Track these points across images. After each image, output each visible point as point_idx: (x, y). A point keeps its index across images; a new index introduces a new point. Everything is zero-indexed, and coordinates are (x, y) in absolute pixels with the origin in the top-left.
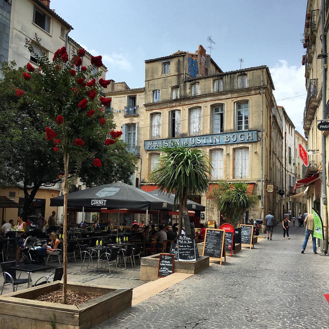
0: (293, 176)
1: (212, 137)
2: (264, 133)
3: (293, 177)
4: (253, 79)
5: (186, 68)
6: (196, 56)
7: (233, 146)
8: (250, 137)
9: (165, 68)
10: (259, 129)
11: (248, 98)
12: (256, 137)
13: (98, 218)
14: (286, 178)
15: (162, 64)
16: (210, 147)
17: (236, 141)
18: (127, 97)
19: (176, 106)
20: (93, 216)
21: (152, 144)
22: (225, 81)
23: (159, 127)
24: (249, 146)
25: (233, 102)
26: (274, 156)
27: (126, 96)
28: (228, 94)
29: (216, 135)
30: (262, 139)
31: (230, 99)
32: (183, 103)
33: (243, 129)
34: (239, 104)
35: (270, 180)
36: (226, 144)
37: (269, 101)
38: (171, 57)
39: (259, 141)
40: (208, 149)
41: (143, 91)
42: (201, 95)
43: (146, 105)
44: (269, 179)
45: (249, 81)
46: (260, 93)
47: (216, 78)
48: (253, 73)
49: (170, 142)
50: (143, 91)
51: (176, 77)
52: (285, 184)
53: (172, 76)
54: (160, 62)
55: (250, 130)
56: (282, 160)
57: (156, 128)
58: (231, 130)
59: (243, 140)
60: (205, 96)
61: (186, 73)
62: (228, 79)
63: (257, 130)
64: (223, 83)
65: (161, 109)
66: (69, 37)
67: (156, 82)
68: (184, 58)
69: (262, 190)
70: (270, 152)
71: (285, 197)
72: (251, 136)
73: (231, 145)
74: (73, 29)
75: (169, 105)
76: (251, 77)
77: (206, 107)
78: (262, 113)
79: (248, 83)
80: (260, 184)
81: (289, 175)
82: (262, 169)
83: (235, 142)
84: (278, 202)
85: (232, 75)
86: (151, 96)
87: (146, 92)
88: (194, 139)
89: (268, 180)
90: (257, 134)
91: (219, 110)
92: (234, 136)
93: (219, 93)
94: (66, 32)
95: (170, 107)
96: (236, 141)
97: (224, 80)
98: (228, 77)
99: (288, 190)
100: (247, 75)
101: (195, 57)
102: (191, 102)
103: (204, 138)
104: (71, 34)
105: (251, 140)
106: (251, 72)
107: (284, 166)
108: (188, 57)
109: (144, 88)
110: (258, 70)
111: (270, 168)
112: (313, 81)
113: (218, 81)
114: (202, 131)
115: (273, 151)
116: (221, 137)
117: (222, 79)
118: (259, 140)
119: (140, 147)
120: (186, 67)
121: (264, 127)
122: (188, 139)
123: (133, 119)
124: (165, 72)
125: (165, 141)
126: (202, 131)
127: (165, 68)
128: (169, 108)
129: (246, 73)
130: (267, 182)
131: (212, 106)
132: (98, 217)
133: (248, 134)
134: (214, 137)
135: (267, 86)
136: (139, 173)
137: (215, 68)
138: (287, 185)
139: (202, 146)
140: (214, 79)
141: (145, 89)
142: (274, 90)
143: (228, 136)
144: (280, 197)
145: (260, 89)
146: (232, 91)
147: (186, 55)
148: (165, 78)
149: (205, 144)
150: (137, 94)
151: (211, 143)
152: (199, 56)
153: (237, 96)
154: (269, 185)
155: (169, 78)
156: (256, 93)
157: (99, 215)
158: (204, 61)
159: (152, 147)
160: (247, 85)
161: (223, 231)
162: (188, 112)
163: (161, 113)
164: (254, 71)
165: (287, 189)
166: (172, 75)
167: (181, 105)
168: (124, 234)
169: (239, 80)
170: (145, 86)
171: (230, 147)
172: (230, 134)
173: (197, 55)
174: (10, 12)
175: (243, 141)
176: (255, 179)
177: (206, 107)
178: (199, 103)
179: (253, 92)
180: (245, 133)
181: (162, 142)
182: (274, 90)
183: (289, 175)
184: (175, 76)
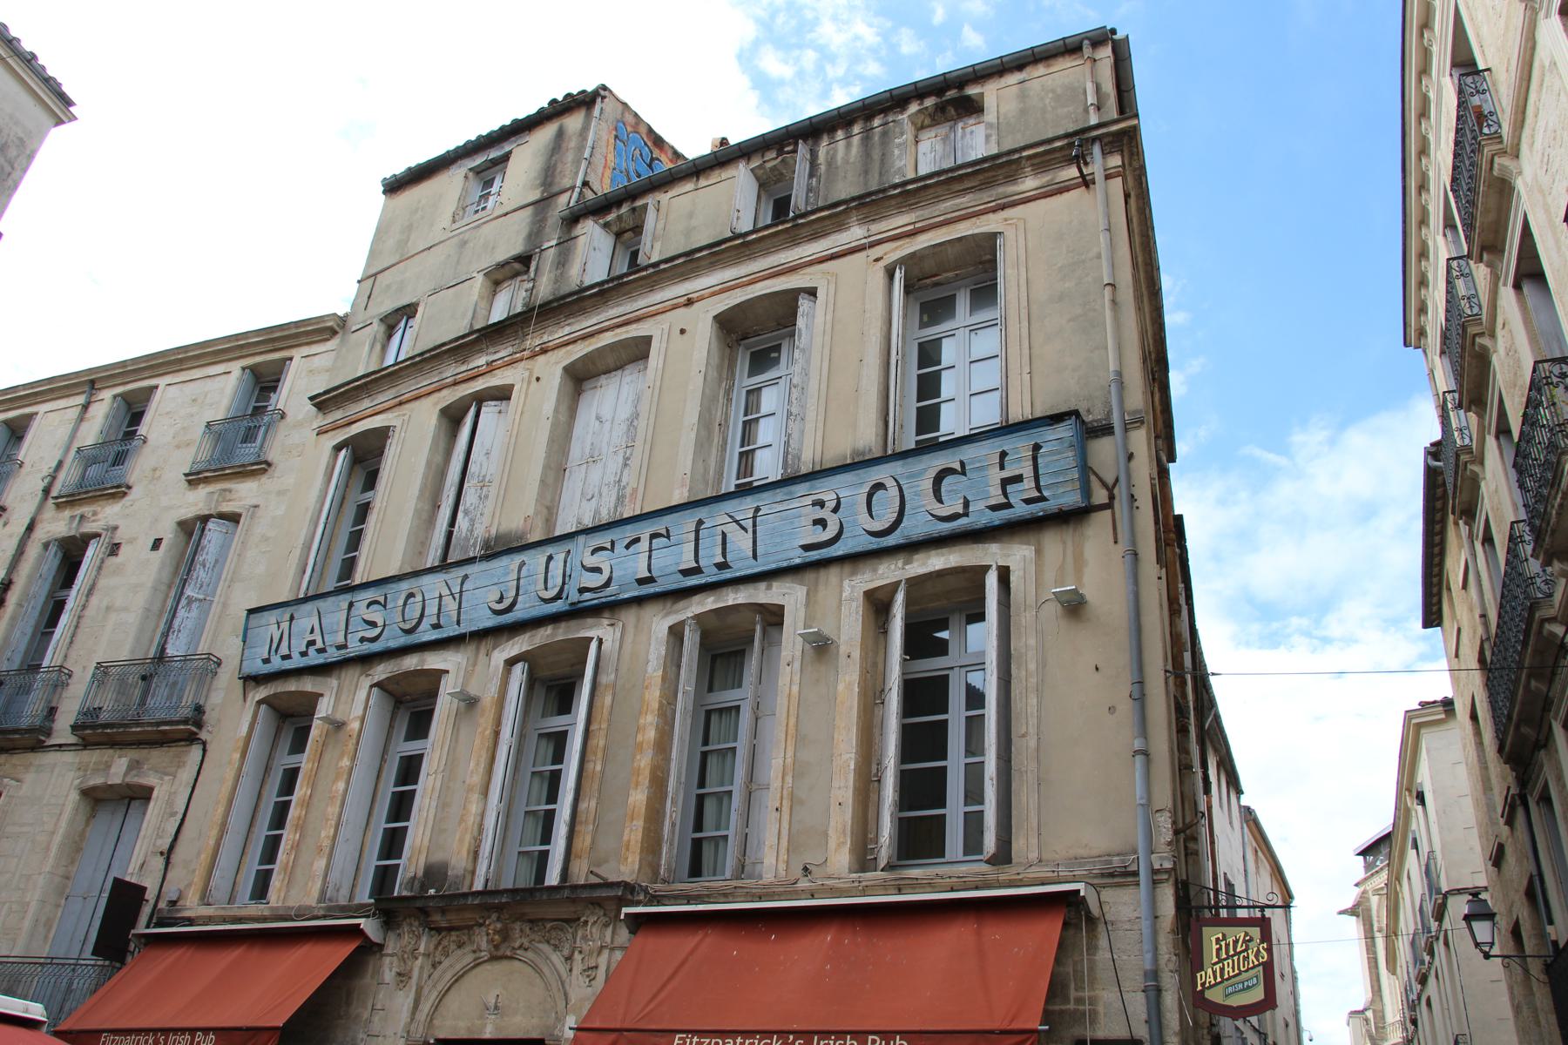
4: (1023, 112)
7: (868, 576)
8: (1018, 479)
10: (1093, 417)
15: (466, 177)
16: (682, 604)
19: (491, 368)
25: (882, 264)
30: (1130, 485)
32: (533, 342)
46: (1086, 182)
62: (848, 146)
69: (1154, 974)
73: (853, 573)
82: (1145, 753)
83: (891, 541)
85: (877, 122)
92: (879, 486)
103: (637, 540)
105: (1028, 501)
114: (635, 490)
118: (1100, 496)
119: (219, 664)
123: (230, 491)
126: (635, 490)
129: (972, 91)
133: (1003, 455)
136: (162, 853)
143: (829, 498)
164: (1028, 69)
168: (1208, 1033)
176: (1076, 860)
177: (683, 331)
178: (638, 320)
179: (1029, 183)
180: (968, 453)
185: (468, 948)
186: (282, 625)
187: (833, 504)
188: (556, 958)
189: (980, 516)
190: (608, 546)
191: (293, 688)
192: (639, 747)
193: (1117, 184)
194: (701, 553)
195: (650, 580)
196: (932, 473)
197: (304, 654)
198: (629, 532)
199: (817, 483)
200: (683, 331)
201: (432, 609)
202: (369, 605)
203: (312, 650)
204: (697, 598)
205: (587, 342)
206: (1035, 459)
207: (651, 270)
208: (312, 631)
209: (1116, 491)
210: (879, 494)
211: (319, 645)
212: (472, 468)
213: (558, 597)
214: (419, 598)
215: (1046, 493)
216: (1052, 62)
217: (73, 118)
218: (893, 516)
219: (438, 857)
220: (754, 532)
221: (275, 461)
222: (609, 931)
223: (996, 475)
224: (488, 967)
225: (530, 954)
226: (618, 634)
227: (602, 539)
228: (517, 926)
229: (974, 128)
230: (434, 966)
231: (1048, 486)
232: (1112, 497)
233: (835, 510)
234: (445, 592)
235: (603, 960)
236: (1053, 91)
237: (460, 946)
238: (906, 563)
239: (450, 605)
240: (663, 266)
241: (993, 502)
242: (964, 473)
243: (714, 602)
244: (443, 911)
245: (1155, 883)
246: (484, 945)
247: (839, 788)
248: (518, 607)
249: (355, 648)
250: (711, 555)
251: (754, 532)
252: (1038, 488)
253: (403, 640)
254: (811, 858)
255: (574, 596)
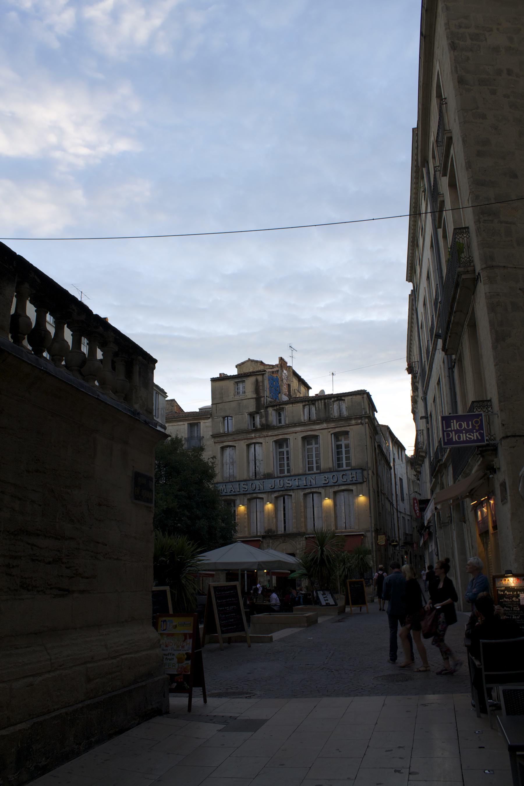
0: (407, 518)
1: (306, 478)
2: (370, 472)
3: (408, 520)
8: (354, 477)
11: (347, 429)
14: (399, 522)
15: (234, 384)
16: (304, 490)
17: (337, 482)
18: (186, 425)
19: (255, 438)
21: (225, 489)
22: (318, 407)
23: (233, 465)
25: (330, 433)
26: (383, 496)
27: (186, 423)
29: (311, 476)
30: (369, 479)
31: (326, 430)
32: (265, 433)
34: (337, 436)
35: (381, 529)
36: (325, 486)
37: (372, 430)
39: (365, 482)
40: (302, 493)
41: (209, 417)
42: (289, 425)
44: (379, 528)
46: (361, 424)
47: (307, 403)
49: (250, 485)
50: (209, 417)
51: (254, 400)
52: (399, 530)
53: (249, 399)
56: (392, 497)
57: (228, 465)
58: (329, 468)
59: (346, 480)
60: (295, 425)
61: (267, 396)
62: (322, 405)
63: (361, 469)
64: (315, 410)
68: (263, 378)
70: (378, 492)
71: (399, 549)
77: (296, 439)
78: (366, 447)
79: (346, 411)
80: (369, 534)
81: (403, 517)
83: (336, 484)
84: (390, 557)
85: (326, 401)
87: (213, 419)
88: (282, 481)
89: (378, 530)
90: (362, 473)
91: (312, 442)
93: (311, 422)
95: (248, 439)
96: (337, 482)
99: (403, 539)
100: (344, 400)
102: (276, 432)
103: (295, 479)
105: (355, 480)
106: (350, 397)
107: (395, 506)
110: (358, 395)
111: (379, 513)
112: (419, 432)
113: (308, 407)
115: (381, 491)
116: (317, 476)
117: (314, 404)
121: (370, 465)
122: (275, 481)
125: (243, 483)
129: (343, 398)
130: (377, 532)
131: (304, 438)
134: (309, 477)
135: (370, 415)
137: (298, 380)
138: (402, 531)
140: (304, 404)
142: (377, 412)
143: (326, 476)
144: (393, 549)
146: (328, 420)
147: (265, 373)
148: (240, 401)
149: (297, 486)
150: (200, 421)
153: (334, 426)
154: (380, 536)
155: (245, 401)
156: (356, 422)
158: (286, 377)
159: (226, 492)
160: (345, 413)
163: (235, 446)
165: (400, 538)
166: (249, 398)
167: (262, 437)
169: (335, 406)
172: (329, 473)
175: (345, 482)
179: (353, 422)
180: (347, 472)
181: (239, 484)
182: (377, 412)
183: (403, 517)
184: (253, 399)
188: (294, 542)
189: (348, 482)
191: (229, 498)
193: (367, 425)
195: (299, 486)
196: (342, 474)
197: (230, 492)
198: (294, 478)
201: (258, 487)
202: (243, 485)
203: (232, 492)
208: (231, 488)
210: (334, 477)
212: (257, 458)
223: (351, 476)
230: (273, 544)
231: (359, 479)
233: (328, 478)
234: (260, 484)
237: (277, 541)
239: (262, 487)
242: (346, 475)
245: (372, 532)
247: (433, 672)
249: (242, 492)
253: (252, 492)
255: (286, 488)
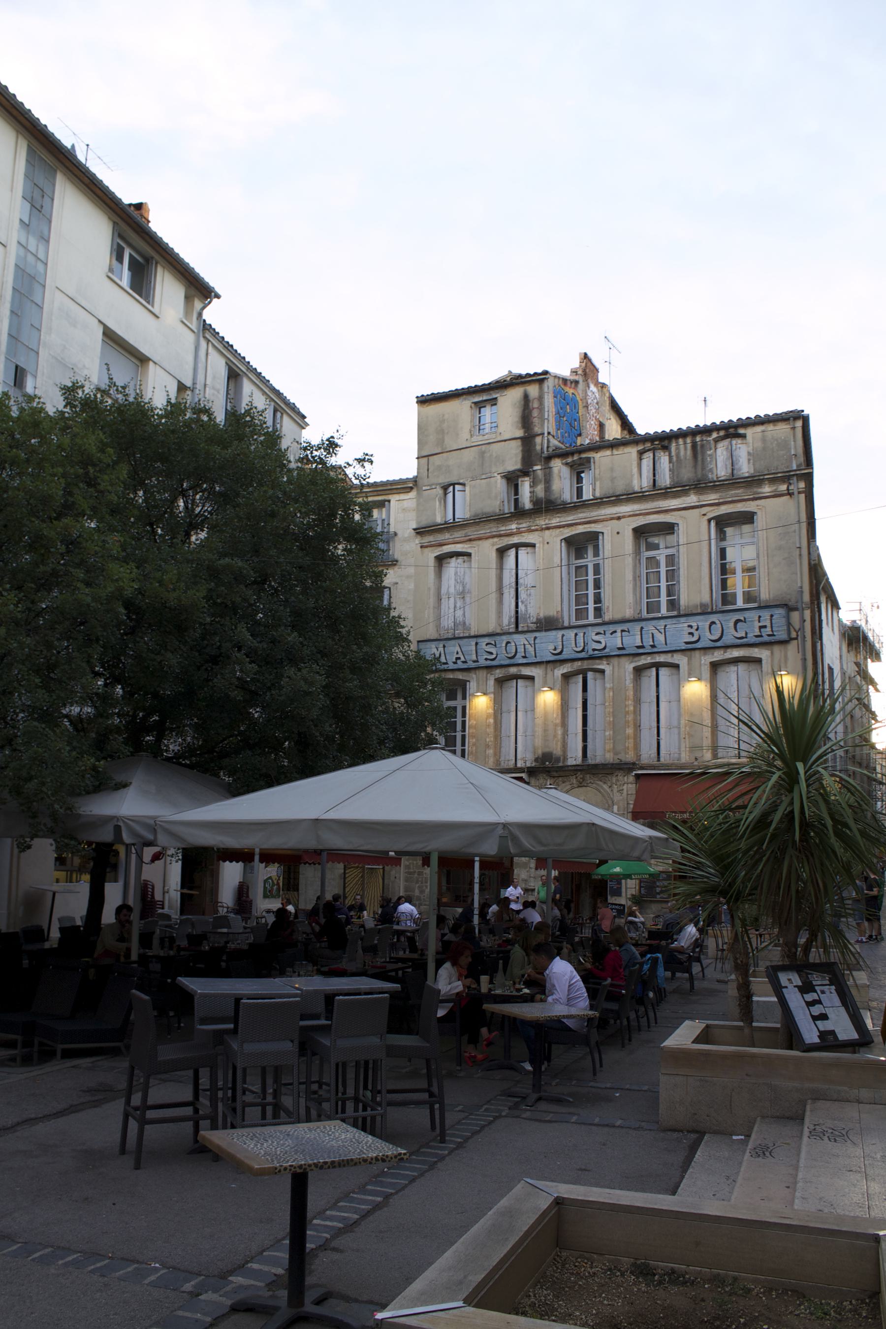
1: (642, 628)
4: (764, 449)
5: (548, 416)
6: (573, 385)
8: (765, 627)
9: (480, 417)
11: (750, 507)
12: (785, 627)
13: (278, 889)
15: (471, 407)
16: (637, 659)
19: (519, 532)
20: (265, 881)
22: (678, 455)
24: (763, 654)
28: (689, 496)
29: (654, 622)
32: (542, 521)
33: (664, 611)
36: (689, 650)
38: (501, 385)
40: (629, 666)
42: (600, 499)
43: (420, 532)
45: (753, 456)
47: (648, 445)
48: (763, 431)
49: (504, 645)
50: (411, 488)
51: (519, 442)
53: (505, 441)
54: (465, 399)
55: (762, 605)
58: (702, 605)
60: (617, 499)
61: (549, 433)
62: (686, 449)
65: (470, 540)
66: (204, 321)
67: (452, 460)
68: (541, 389)
72: (768, 624)
73: (705, 654)
74: (218, 296)
75: (492, 528)
76: (759, 445)
83: (718, 644)
85: (698, 439)
86: (437, 503)
90: (788, 618)
92: (713, 623)
93: (657, 492)
94: (198, 304)
95: (500, 536)
97: (673, 453)
98: (685, 443)
100: (743, 436)
101: (570, 388)
102: (570, 518)
103: (615, 632)
104: (213, 314)
105: (769, 635)
106: (759, 429)
108: (555, 386)
109: (415, 480)
110: (780, 424)
117: (666, 448)
118: (794, 635)
120: (550, 414)
122: (563, 636)
124: (479, 430)
125: (487, 640)
127: (480, 417)
128: (496, 540)
132: (278, 884)
133: (760, 617)
137: (620, 422)
139: (608, 657)
141: (416, 481)
143: (694, 625)
145: (789, 480)
146: (701, 485)
148: (483, 447)
149: (619, 649)
150: (390, 497)
151: (638, 647)
152: (581, 385)
153: (717, 501)
156: (775, 491)
157: (281, 878)
160: (745, 468)
161: (265, 896)
162: (497, 557)
163: (469, 555)
167: (537, 530)
169: (719, 451)
170: (418, 472)
171: (701, 661)
173: (577, 382)
174: (47, 241)
179: (767, 489)
180: (747, 614)
181: (477, 644)
185: (568, 783)
186: (439, 649)
187: (696, 627)
189: (751, 639)
190: (603, 632)
192: (627, 713)
194: (644, 640)
196: (733, 620)
197: (455, 663)
198: (612, 628)
199: (689, 618)
200: (618, 533)
201: (521, 650)
203: (459, 661)
204: (643, 657)
205: (570, 529)
206: (771, 620)
207: (599, 501)
209: (799, 633)
210: (713, 626)
211: (463, 659)
212: (520, 581)
213: (583, 651)
214: (513, 644)
215: (775, 633)
216: (776, 423)
217: (307, 425)
218: (719, 635)
219: (547, 750)
220: (665, 635)
221: (399, 559)
222: (626, 778)
223: (757, 624)
224: (577, 789)
225: (594, 785)
226: (611, 668)
227: (600, 629)
228: (588, 776)
229: (740, 445)
232: (797, 636)
233: (697, 630)
234: (526, 643)
235: (625, 787)
236: (777, 440)
238: (724, 652)
240: (605, 500)
241: (756, 634)
243: (651, 659)
244: (557, 771)
246: (575, 782)
248: (564, 653)
249: (483, 662)
250: (648, 642)
251: (665, 635)
252: (772, 631)
253: (507, 662)
254: (698, 755)
255: (591, 652)
